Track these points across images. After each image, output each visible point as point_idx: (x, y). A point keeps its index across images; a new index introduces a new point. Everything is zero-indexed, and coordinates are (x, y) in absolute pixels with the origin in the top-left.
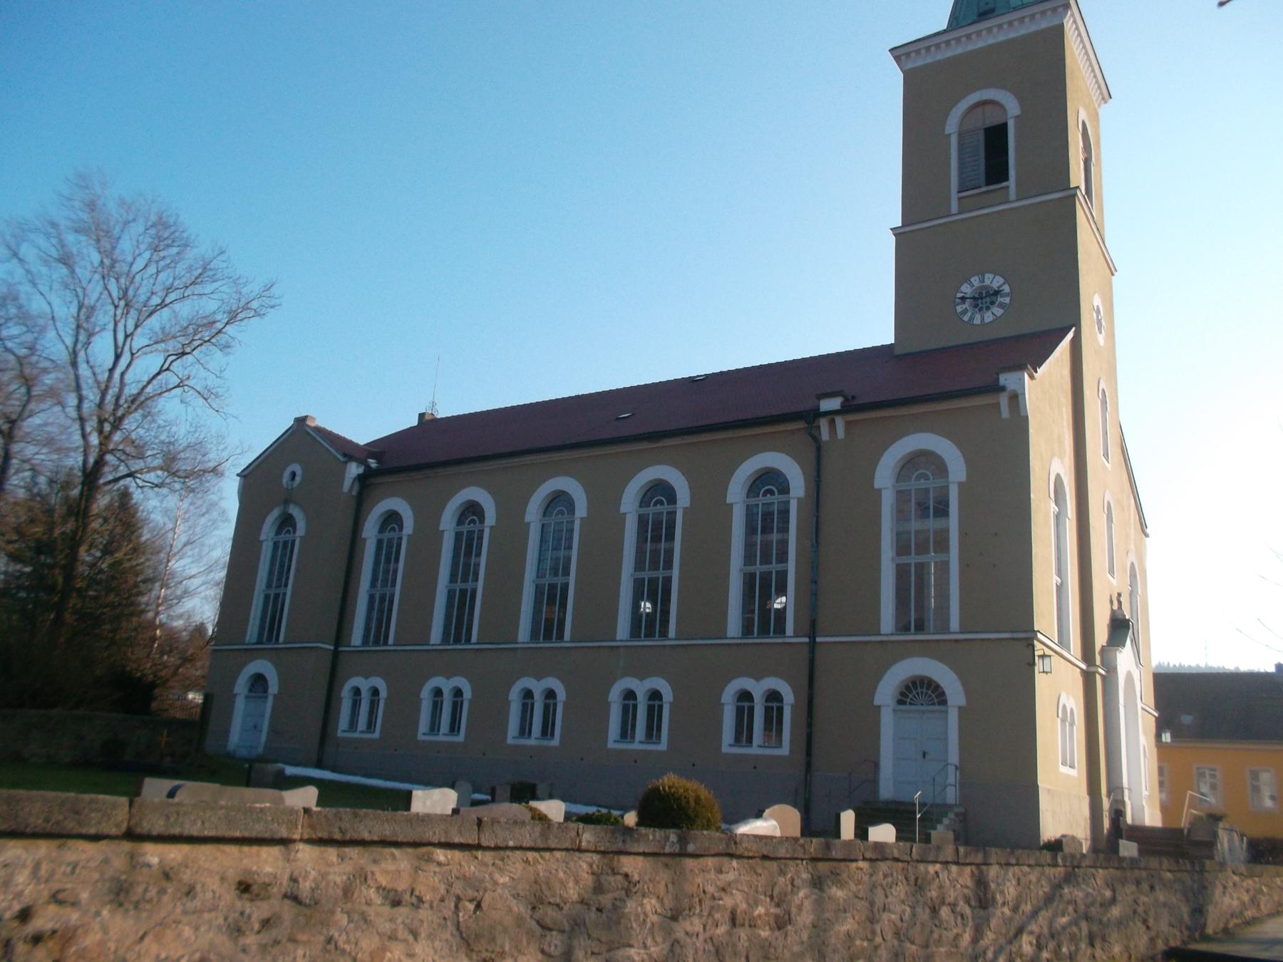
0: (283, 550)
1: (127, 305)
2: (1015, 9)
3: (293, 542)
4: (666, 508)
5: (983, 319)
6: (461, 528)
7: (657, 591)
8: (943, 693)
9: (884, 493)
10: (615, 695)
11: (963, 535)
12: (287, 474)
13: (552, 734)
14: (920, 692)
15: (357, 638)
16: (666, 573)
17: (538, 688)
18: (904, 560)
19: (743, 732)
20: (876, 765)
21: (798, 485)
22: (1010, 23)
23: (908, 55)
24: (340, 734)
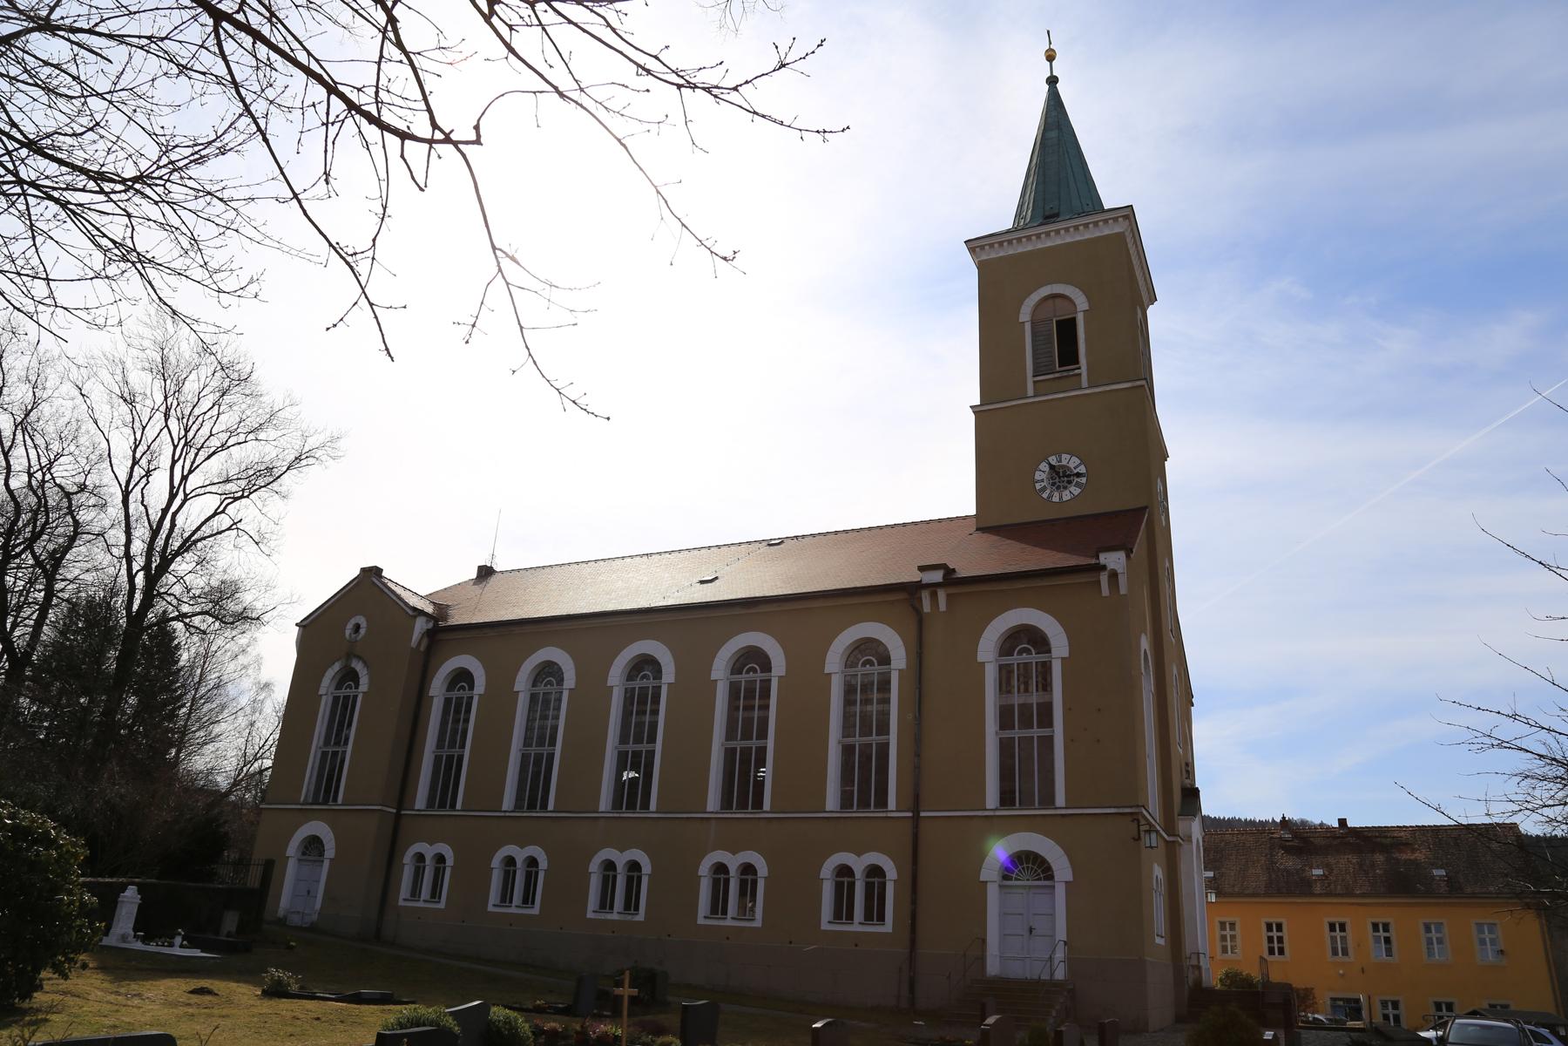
0: (343, 709)
1: (186, 444)
2: (1079, 215)
3: (355, 697)
4: (759, 676)
6: (536, 690)
7: (641, 762)
8: (1049, 868)
10: (705, 868)
12: (350, 626)
13: (637, 908)
15: (420, 802)
16: (760, 743)
17: (521, 854)
18: (1007, 734)
19: (843, 910)
20: (984, 941)
23: (982, 248)
24: (401, 903)
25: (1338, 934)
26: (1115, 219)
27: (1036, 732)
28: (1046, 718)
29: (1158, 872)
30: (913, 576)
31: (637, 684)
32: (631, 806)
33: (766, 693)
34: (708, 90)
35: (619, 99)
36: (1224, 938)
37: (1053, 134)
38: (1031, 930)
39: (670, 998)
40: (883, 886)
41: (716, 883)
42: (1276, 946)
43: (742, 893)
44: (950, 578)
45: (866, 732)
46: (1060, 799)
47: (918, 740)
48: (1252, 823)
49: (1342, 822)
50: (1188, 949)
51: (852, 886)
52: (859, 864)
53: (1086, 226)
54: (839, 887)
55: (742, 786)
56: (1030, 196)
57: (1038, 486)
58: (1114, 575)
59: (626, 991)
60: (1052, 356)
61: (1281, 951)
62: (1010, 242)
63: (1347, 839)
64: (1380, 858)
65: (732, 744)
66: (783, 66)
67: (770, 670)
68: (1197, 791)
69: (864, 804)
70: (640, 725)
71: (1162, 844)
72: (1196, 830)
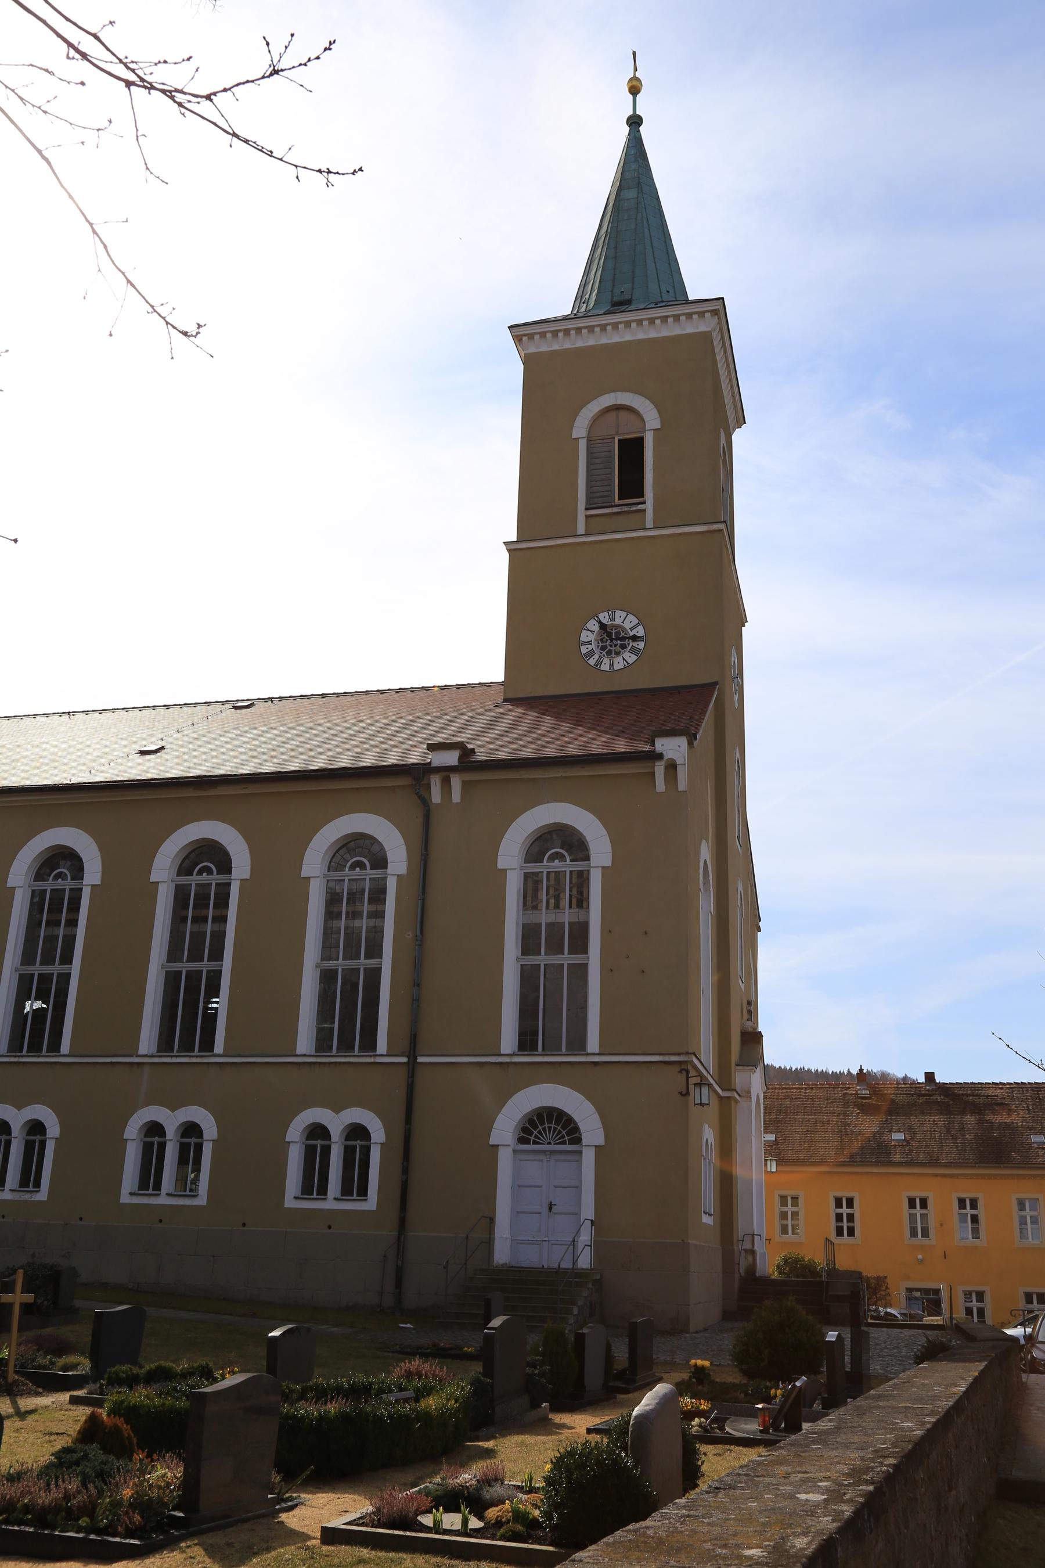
2: (657, 305)
4: (215, 879)
5: (612, 665)
7: (53, 990)
8: (576, 1129)
9: (509, 874)
10: (133, 1129)
11: (607, 931)
13: (37, 1184)
14: (549, 1127)
16: (214, 965)
18: (531, 960)
19: (314, 1182)
20: (492, 1220)
21: (398, 859)
22: (652, 321)
23: (531, 336)
25: (918, 1211)
26: (702, 314)
27: (566, 959)
28: (580, 943)
29: (709, 1134)
30: (417, 755)
31: (49, 885)
32: (35, 1047)
33: (223, 901)
34: (169, 94)
35: (39, 88)
36: (784, 1216)
37: (631, 194)
38: (551, 1206)
39: (78, 1303)
40: (366, 1151)
41: (147, 1148)
42: (845, 1226)
43: (183, 1160)
44: (468, 761)
45: (352, 952)
46: (593, 1043)
47: (418, 964)
48: (823, 1075)
49: (930, 1076)
50: (741, 1228)
51: (326, 1151)
52: (336, 1123)
53: (664, 319)
54: (309, 1153)
55: (187, 1020)
56: (596, 275)
57: (584, 650)
58: (672, 767)
59: (18, 1297)
60: (611, 485)
61: (851, 1232)
62: (567, 332)
63: (936, 1098)
64: (970, 1120)
65: (175, 966)
66: (276, 72)
67: (229, 871)
68: (759, 1036)
69: (346, 1045)
70: (51, 940)
71: (714, 1101)
72: (756, 1083)
